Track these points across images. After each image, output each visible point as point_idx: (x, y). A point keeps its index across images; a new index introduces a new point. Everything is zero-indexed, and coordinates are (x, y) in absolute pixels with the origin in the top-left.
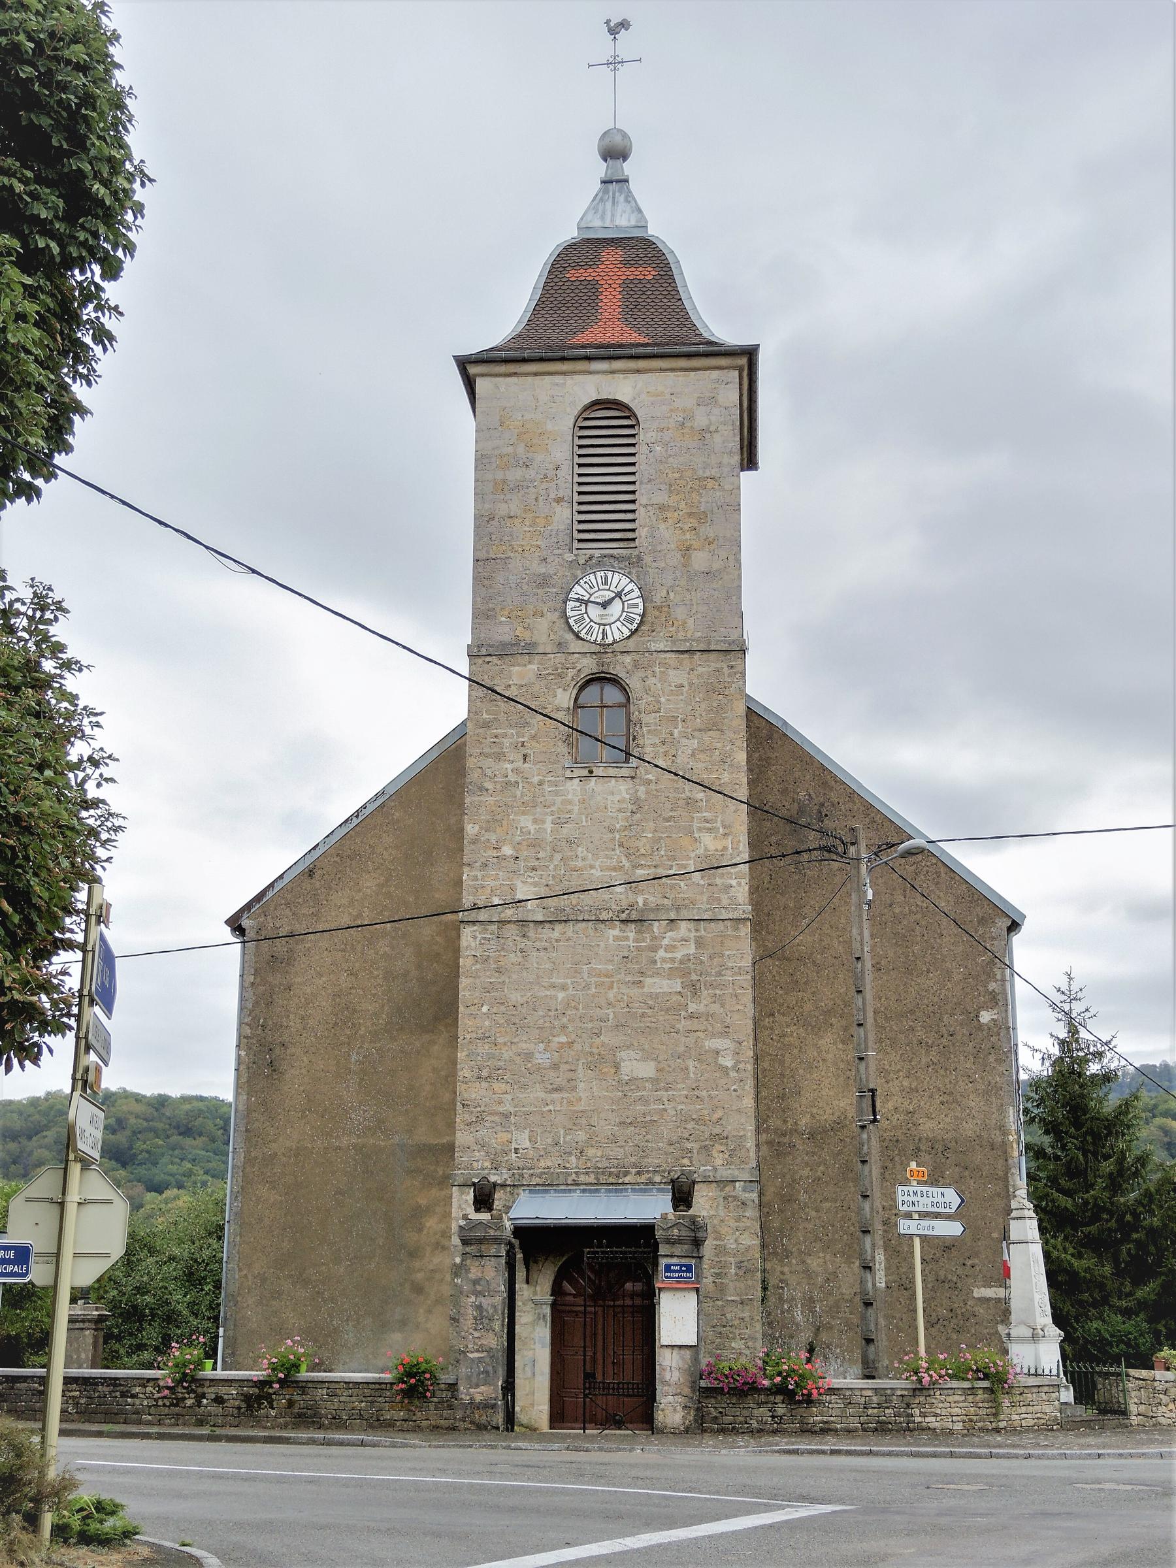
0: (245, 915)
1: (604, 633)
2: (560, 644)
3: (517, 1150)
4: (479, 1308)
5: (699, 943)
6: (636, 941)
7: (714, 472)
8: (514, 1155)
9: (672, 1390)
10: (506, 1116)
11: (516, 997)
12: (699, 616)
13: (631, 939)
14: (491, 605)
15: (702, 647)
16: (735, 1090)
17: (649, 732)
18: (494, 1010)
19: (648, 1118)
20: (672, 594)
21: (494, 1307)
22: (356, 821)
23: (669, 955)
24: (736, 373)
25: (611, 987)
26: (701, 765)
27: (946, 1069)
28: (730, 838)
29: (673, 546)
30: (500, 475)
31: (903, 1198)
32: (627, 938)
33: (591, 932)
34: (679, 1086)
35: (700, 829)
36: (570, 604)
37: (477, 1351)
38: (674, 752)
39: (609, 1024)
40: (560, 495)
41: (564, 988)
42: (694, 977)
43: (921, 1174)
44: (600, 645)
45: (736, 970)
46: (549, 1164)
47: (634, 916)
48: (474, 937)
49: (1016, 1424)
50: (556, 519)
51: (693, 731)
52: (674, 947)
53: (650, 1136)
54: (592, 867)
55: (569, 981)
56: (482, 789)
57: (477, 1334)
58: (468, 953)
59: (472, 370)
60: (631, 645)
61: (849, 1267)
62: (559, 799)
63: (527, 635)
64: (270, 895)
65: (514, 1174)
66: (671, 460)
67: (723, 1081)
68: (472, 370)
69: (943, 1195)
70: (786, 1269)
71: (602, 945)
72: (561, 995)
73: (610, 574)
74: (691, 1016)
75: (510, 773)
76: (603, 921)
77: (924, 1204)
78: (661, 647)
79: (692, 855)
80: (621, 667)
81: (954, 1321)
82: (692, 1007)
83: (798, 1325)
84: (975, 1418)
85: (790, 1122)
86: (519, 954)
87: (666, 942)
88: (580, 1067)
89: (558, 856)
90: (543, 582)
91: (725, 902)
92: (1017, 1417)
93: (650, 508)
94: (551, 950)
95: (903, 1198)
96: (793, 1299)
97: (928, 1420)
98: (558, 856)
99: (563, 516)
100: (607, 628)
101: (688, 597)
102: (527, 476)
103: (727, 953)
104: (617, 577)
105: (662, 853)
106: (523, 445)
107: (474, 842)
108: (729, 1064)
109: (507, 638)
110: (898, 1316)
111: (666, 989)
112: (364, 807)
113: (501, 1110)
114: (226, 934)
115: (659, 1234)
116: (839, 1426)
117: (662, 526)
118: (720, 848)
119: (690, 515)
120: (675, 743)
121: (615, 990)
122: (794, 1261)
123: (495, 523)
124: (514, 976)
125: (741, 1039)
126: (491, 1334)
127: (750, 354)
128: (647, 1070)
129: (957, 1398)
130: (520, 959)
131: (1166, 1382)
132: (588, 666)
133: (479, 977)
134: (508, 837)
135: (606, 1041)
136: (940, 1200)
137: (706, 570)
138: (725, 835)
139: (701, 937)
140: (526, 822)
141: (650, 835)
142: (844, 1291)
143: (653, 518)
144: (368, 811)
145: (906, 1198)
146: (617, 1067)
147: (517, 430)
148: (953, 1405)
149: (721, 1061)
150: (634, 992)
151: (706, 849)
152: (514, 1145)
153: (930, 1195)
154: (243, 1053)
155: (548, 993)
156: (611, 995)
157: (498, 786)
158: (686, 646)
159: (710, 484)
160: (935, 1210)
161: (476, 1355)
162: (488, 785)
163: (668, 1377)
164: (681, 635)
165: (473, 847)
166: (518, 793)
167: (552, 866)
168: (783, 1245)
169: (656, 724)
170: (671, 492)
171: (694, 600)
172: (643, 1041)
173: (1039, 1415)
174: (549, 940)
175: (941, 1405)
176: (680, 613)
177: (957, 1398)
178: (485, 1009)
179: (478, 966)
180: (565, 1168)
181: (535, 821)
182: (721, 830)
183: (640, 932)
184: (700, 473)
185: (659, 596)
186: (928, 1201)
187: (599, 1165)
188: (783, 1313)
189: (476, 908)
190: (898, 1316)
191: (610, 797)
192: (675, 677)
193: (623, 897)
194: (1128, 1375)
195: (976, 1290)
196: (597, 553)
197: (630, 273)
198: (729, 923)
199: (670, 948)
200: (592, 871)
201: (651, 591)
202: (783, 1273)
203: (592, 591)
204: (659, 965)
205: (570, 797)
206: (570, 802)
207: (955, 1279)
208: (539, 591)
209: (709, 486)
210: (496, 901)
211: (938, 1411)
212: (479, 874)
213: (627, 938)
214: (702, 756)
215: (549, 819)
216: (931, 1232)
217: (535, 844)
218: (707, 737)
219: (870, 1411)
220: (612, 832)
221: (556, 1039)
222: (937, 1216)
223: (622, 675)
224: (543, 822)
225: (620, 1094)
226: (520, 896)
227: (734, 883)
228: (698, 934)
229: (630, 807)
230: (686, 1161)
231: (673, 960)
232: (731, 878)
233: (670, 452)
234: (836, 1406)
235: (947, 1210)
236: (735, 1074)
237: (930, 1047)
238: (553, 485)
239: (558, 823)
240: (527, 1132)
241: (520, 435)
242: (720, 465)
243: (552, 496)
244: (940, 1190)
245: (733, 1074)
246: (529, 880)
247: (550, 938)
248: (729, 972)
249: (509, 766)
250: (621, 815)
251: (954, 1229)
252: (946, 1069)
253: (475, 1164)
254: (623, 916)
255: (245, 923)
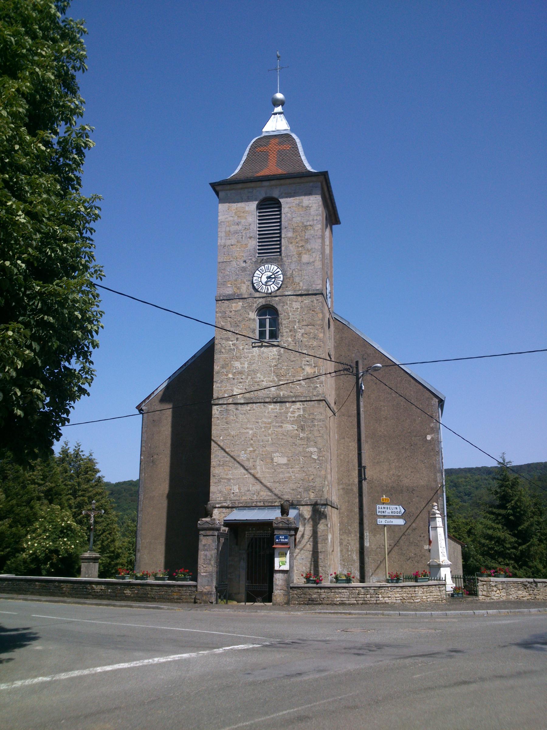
0: (144, 404)
1: (268, 289)
2: (251, 294)
3: (233, 493)
4: (206, 555)
5: (304, 410)
6: (280, 410)
7: (311, 223)
8: (232, 495)
9: (279, 588)
10: (229, 480)
11: (233, 433)
12: (305, 280)
13: (278, 409)
14: (224, 280)
15: (305, 293)
16: (318, 468)
17: (285, 327)
18: (225, 438)
19: (284, 480)
20: (294, 272)
21: (212, 556)
22: (184, 367)
23: (292, 415)
24: (320, 184)
25: (270, 428)
26: (305, 339)
27: (413, 458)
28: (317, 368)
29: (295, 253)
30: (228, 229)
31: (379, 510)
32: (276, 409)
33: (263, 407)
34: (296, 467)
35: (305, 365)
36: (255, 278)
37: (205, 573)
38: (295, 335)
39: (269, 443)
40: (251, 236)
41: (252, 429)
42: (302, 423)
43: (387, 500)
44: (266, 293)
45: (319, 420)
46: (246, 498)
47: (279, 400)
48: (218, 410)
49: (424, 600)
50: (249, 245)
51: (303, 326)
52: (295, 412)
53: (285, 487)
54: (263, 381)
55: (254, 426)
56: (221, 352)
57: (204, 566)
58: (215, 416)
59: (218, 188)
60: (278, 293)
61: (374, 537)
62: (250, 355)
63: (238, 291)
64: (152, 396)
65: (232, 502)
66: (294, 219)
67: (313, 464)
68: (218, 188)
69: (396, 508)
70: (350, 539)
71: (267, 411)
72: (251, 432)
73: (270, 266)
74: (301, 439)
75: (231, 345)
76: (267, 403)
77: (388, 512)
78: (289, 293)
79: (302, 375)
80: (275, 301)
81: (416, 558)
82: (302, 435)
83: (354, 560)
84: (406, 598)
85: (351, 480)
86: (235, 416)
87: (291, 410)
88: (258, 460)
89: (250, 377)
90: (244, 269)
91: (315, 393)
92: (425, 597)
93: (286, 239)
94: (247, 414)
95: (379, 510)
96: (353, 550)
97: (385, 599)
98: (250, 377)
99: (254, 244)
100: (269, 287)
101: (300, 273)
102: (238, 229)
103: (315, 413)
104: (273, 266)
105: (290, 375)
106: (237, 217)
107: (218, 373)
108: (316, 458)
109: (230, 293)
110: (394, 556)
111: (291, 428)
112: (188, 362)
113: (227, 477)
114: (137, 412)
115: (275, 525)
116: (347, 602)
117: (290, 246)
118: (313, 372)
119: (302, 240)
120: (295, 331)
121: (272, 429)
122: (353, 535)
123: (226, 247)
124: (233, 425)
125: (321, 447)
126: (210, 566)
127: (325, 175)
128: (284, 460)
129: (398, 590)
130: (235, 418)
131: (496, 582)
132: (262, 302)
133: (219, 425)
134: (231, 370)
135: (268, 449)
136: (395, 510)
137: (308, 262)
138: (315, 367)
139: (305, 407)
140: (237, 364)
141: (285, 368)
142: (372, 547)
143: (287, 243)
144: (189, 363)
145: (380, 510)
146: (272, 459)
147: (234, 211)
148: (396, 593)
149: (313, 456)
150: (280, 429)
151: (307, 373)
152: (232, 491)
153: (391, 508)
154: (142, 457)
155: (245, 431)
156: (270, 432)
157: (227, 351)
158: (299, 293)
159: (309, 228)
160: (393, 514)
161: (204, 574)
162: (223, 350)
163: (278, 583)
164: (298, 288)
165: (217, 375)
166: (235, 353)
167: (247, 381)
168: (348, 529)
169: (288, 324)
170: (294, 232)
171: (303, 274)
172: (282, 449)
173: (435, 596)
174: (246, 410)
175: (391, 593)
176: (297, 280)
177: (398, 590)
178: (221, 438)
179: (219, 421)
180: (252, 500)
181: (241, 364)
182: (313, 365)
183: (281, 406)
184: (305, 224)
185: (288, 274)
186: (388, 511)
187: (265, 498)
188: (348, 556)
189: (218, 399)
190: (394, 556)
191: (270, 354)
192: (296, 305)
193: (275, 392)
194: (478, 580)
195: (425, 546)
196: (265, 258)
197: (281, 147)
198: (316, 402)
199: (293, 412)
200: (263, 383)
201: (286, 271)
202: (348, 540)
203: (263, 273)
204: (288, 419)
205: (254, 354)
206: (254, 356)
207: (416, 542)
208: (243, 274)
209: (309, 228)
210: (226, 396)
211: (390, 595)
212: (219, 385)
213: (276, 409)
214: (306, 336)
215: (246, 363)
216: (391, 524)
217: (241, 373)
218: (308, 329)
219: (360, 596)
220: (270, 367)
221: (249, 449)
222: (393, 517)
223: (275, 305)
224: (244, 364)
225: (273, 470)
226: (235, 393)
227: (318, 386)
228: (304, 406)
229: (278, 357)
230: (299, 497)
231: (294, 417)
232: (317, 384)
233: (293, 216)
234: (346, 594)
235: (399, 514)
236: (318, 461)
237: (406, 449)
238: (248, 231)
239: (250, 364)
240: (237, 486)
241: (236, 213)
242: (313, 220)
243: (248, 236)
244: (395, 506)
245: (317, 461)
246: (239, 387)
247: (247, 409)
248: (316, 421)
249: (231, 343)
250: (274, 361)
251: (401, 522)
252: (413, 458)
253: (217, 499)
254: (275, 400)
255: (144, 408)
